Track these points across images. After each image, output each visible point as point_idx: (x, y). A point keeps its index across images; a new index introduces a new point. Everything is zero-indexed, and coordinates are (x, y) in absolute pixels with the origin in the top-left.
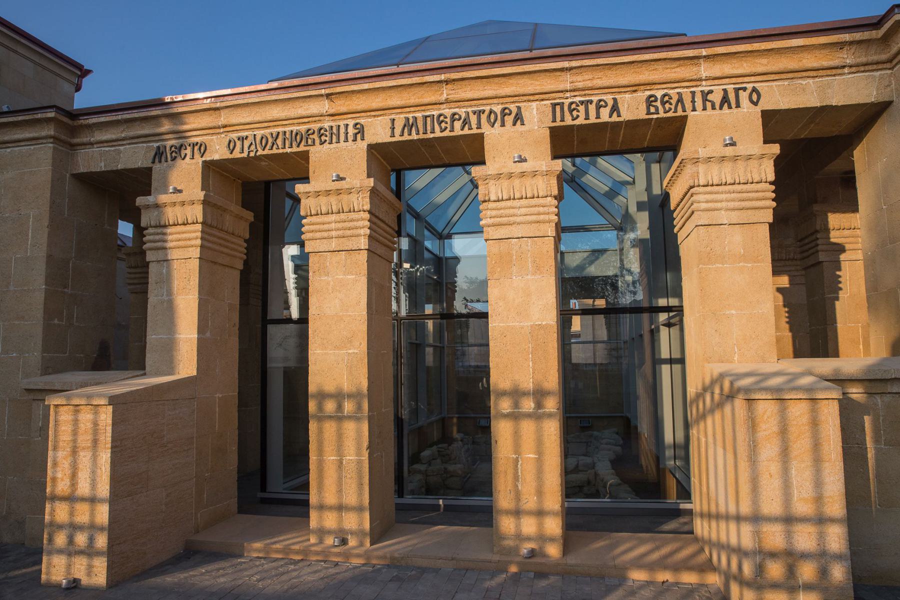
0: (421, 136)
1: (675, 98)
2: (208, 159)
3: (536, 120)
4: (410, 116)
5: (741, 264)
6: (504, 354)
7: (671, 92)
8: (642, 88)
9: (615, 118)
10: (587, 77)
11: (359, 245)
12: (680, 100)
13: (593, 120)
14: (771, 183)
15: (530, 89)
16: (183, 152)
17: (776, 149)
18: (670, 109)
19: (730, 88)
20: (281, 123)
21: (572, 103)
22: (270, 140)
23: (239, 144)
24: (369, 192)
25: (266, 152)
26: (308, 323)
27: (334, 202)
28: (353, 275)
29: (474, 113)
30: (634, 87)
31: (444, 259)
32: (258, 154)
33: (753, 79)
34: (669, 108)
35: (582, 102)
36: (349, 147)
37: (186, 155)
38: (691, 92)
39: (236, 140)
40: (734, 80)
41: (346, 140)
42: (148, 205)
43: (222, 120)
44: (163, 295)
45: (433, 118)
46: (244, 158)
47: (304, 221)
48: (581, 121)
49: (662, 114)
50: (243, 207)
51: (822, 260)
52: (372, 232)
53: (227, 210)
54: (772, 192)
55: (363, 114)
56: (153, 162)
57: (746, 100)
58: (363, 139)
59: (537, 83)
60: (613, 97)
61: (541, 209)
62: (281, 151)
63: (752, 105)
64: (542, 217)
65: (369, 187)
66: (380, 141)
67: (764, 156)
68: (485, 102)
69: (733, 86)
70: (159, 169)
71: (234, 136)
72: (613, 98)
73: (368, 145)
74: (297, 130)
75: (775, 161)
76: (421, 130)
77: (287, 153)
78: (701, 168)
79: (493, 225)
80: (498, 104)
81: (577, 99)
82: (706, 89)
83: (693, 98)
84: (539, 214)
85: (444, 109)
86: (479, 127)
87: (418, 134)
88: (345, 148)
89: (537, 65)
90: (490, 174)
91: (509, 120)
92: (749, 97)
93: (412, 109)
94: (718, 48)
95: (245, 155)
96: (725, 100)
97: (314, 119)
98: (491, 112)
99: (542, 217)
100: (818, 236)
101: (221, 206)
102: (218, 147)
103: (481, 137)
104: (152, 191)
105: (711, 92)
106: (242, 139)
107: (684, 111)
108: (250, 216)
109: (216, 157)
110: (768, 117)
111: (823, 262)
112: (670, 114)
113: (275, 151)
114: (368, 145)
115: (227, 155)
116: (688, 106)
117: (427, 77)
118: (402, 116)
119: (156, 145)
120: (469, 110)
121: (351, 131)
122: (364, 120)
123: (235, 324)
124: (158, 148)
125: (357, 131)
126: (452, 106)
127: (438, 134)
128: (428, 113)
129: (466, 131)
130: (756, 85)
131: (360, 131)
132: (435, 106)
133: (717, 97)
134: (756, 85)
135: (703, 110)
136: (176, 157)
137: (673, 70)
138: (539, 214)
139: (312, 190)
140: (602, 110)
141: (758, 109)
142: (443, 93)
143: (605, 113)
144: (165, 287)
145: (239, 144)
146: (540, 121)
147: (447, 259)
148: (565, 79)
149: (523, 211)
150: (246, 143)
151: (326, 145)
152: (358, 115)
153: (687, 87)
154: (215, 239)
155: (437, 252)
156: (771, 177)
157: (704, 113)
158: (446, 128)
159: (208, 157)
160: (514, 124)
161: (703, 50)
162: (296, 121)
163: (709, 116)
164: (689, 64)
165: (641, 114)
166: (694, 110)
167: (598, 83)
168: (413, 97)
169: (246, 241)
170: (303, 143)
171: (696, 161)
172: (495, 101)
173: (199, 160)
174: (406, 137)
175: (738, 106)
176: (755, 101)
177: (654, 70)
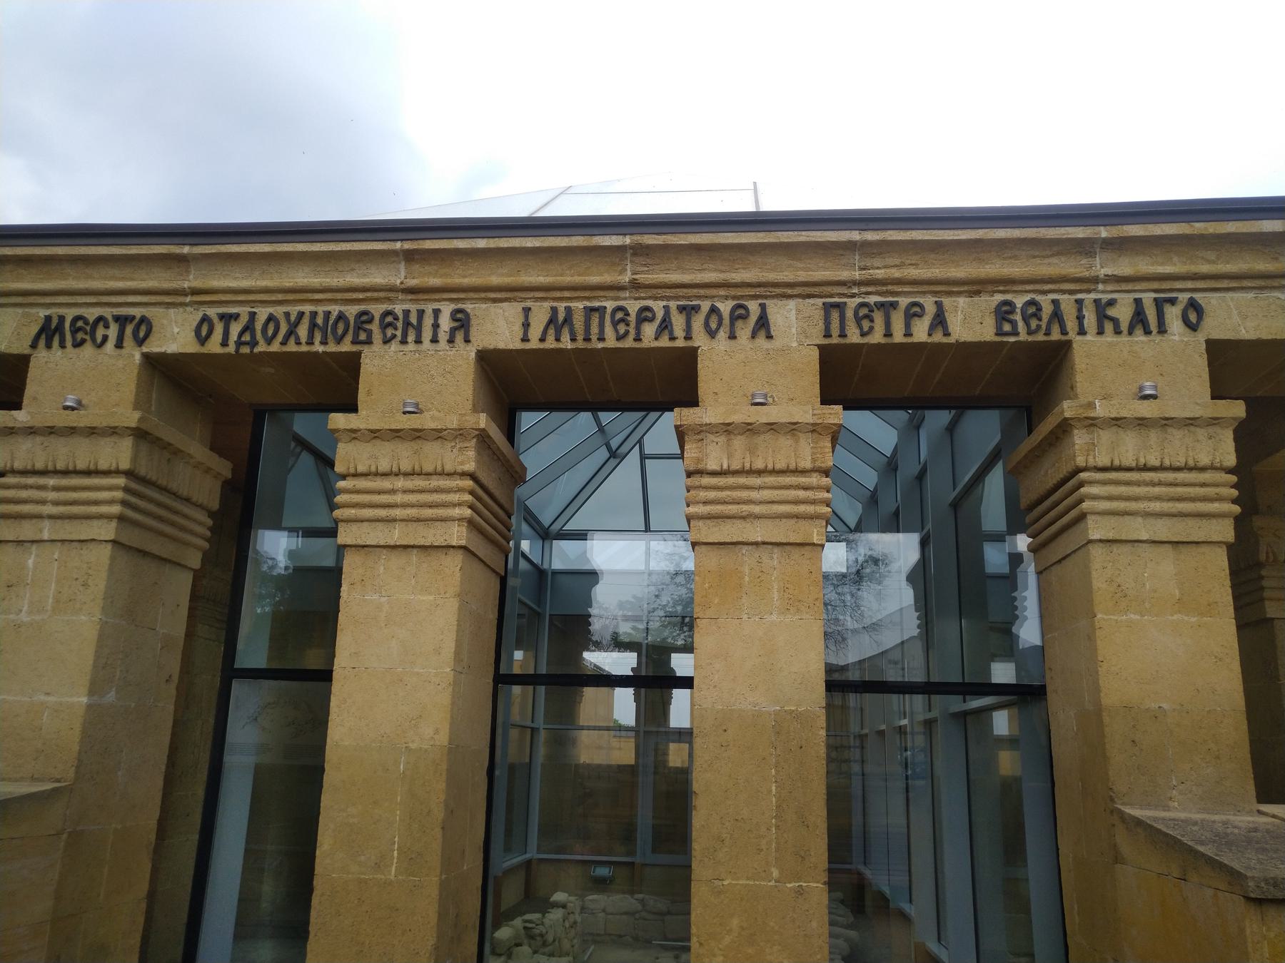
0: (580, 344)
1: (1047, 310)
2: (156, 350)
3: (794, 330)
4: (561, 306)
5: (1175, 617)
6: (721, 767)
7: (1039, 298)
8: (990, 288)
9: (938, 337)
10: (890, 261)
11: (447, 537)
12: (1057, 315)
13: (898, 337)
14: (1230, 471)
15: (786, 276)
16: (100, 332)
17: (1237, 409)
18: (1039, 327)
19: (1148, 298)
20: (310, 296)
21: (862, 305)
22: (284, 329)
23: (219, 329)
24: (475, 440)
25: (275, 347)
26: (331, 680)
27: (404, 455)
28: (430, 594)
29: (682, 309)
30: (976, 287)
31: (550, 574)
32: (257, 349)
33: (1190, 285)
34: (1037, 326)
35: (881, 306)
36: (441, 353)
37: (105, 338)
38: (1076, 301)
39: (216, 320)
40: (1156, 285)
41: (435, 340)
42: (13, 428)
43: (193, 280)
44: (21, 611)
45: (605, 312)
46: (229, 354)
47: (341, 484)
48: (877, 337)
49: (1023, 336)
50: (212, 449)
51: (1273, 616)
52: (474, 514)
53: (182, 451)
54: (1232, 487)
55: (472, 295)
56: (34, 345)
57: (1177, 321)
58: (467, 341)
59: (800, 265)
60: (937, 299)
61: (802, 494)
62: (304, 348)
63: (1188, 330)
64: (802, 508)
65: (476, 430)
66: (501, 346)
67: (1215, 422)
68: (702, 292)
69: (1154, 295)
70: (45, 359)
71: (212, 312)
72: (936, 302)
73: (478, 351)
74: (340, 312)
75: (1235, 432)
76: (580, 337)
77: (316, 353)
78: (1105, 436)
79: (710, 517)
80: (726, 298)
81: (873, 299)
82: (1105, 297)
83: (1080, 310)
84: (797, 502)
85: (625, 299)
86: (688, 337)
87: (573, 340)
88: (433, 352)
89: (804, 233)
90: (708, 422)
91: (744, 330)
92: (1183, 316)
93: (567, 294)
94: (1130, 227)
95: (231, 349)
96: (1139, 318)
97: (376, 295)
98: (714, 310)
99: (802, 508)
100: (1264, 573)
101: (170, 444)
102: (176, 330)
103: (691, 355)
104: (25, 402)
105: (1111, 303)
106: (227, 319)
107: (1064, 332)
108: (224, 468)
109: (172, 348)
110: (1219, 353)
111: (1273, 619)
112: (1040, 337)
113: (292, 347)
114: (478, 351)
115: (191, 347)
116: (1071, 325)
117: (598, 237)
118: (547, 305)
119: (43, 313)
120: (673, 305)
121: (445, 323)
122: (473, 306)
123: (170, 677)
124: (48, 319)
125: (456, 324)
126: (642, 295)
127: (611, 342)
128: (596, 304)
129: (664, 342)
130: (1197, 296)
131: (462, 323)
132: (611, 294)
133: (1123, 312)
134: (1197, 296)
135: (1098, 333)
136: (83, 342)
137: (1046, 261)
138: (797, 502)
139: (362, 426)
140: (916, 321)
141: (1201, 337)
142: (626, 270)
143: (921, 332)
144: (28, 595)
145: (219, 329)
146: (804, 333)
147: (555, 573)
148: (852, 261)
149: (766, 494)
150: (235, 329)
151: (394, 346)
152: (462, 296)
153: (1071, 292)
154: (151, 507)
155: (537, 560)
156: (1231, 460)
157: (1099, 338)
158: (627, 333)
159: (154, 347)
160: (754, 336)
161: (1102, 228)
162: (339, 296)
163: (1111, 345)
164: (1075, 251)
165: (985, 331)
166: (1082, 332)
167: (914, 273)
168: (568, 272)
169: (211, 514)
170: (349, 337)
171: (1092, 424)
172: (722, 292)
173: (135, 355)
174: (550, 344)
175: (1162, 330)
176: (1195, 322)
177: (1010, 258)
